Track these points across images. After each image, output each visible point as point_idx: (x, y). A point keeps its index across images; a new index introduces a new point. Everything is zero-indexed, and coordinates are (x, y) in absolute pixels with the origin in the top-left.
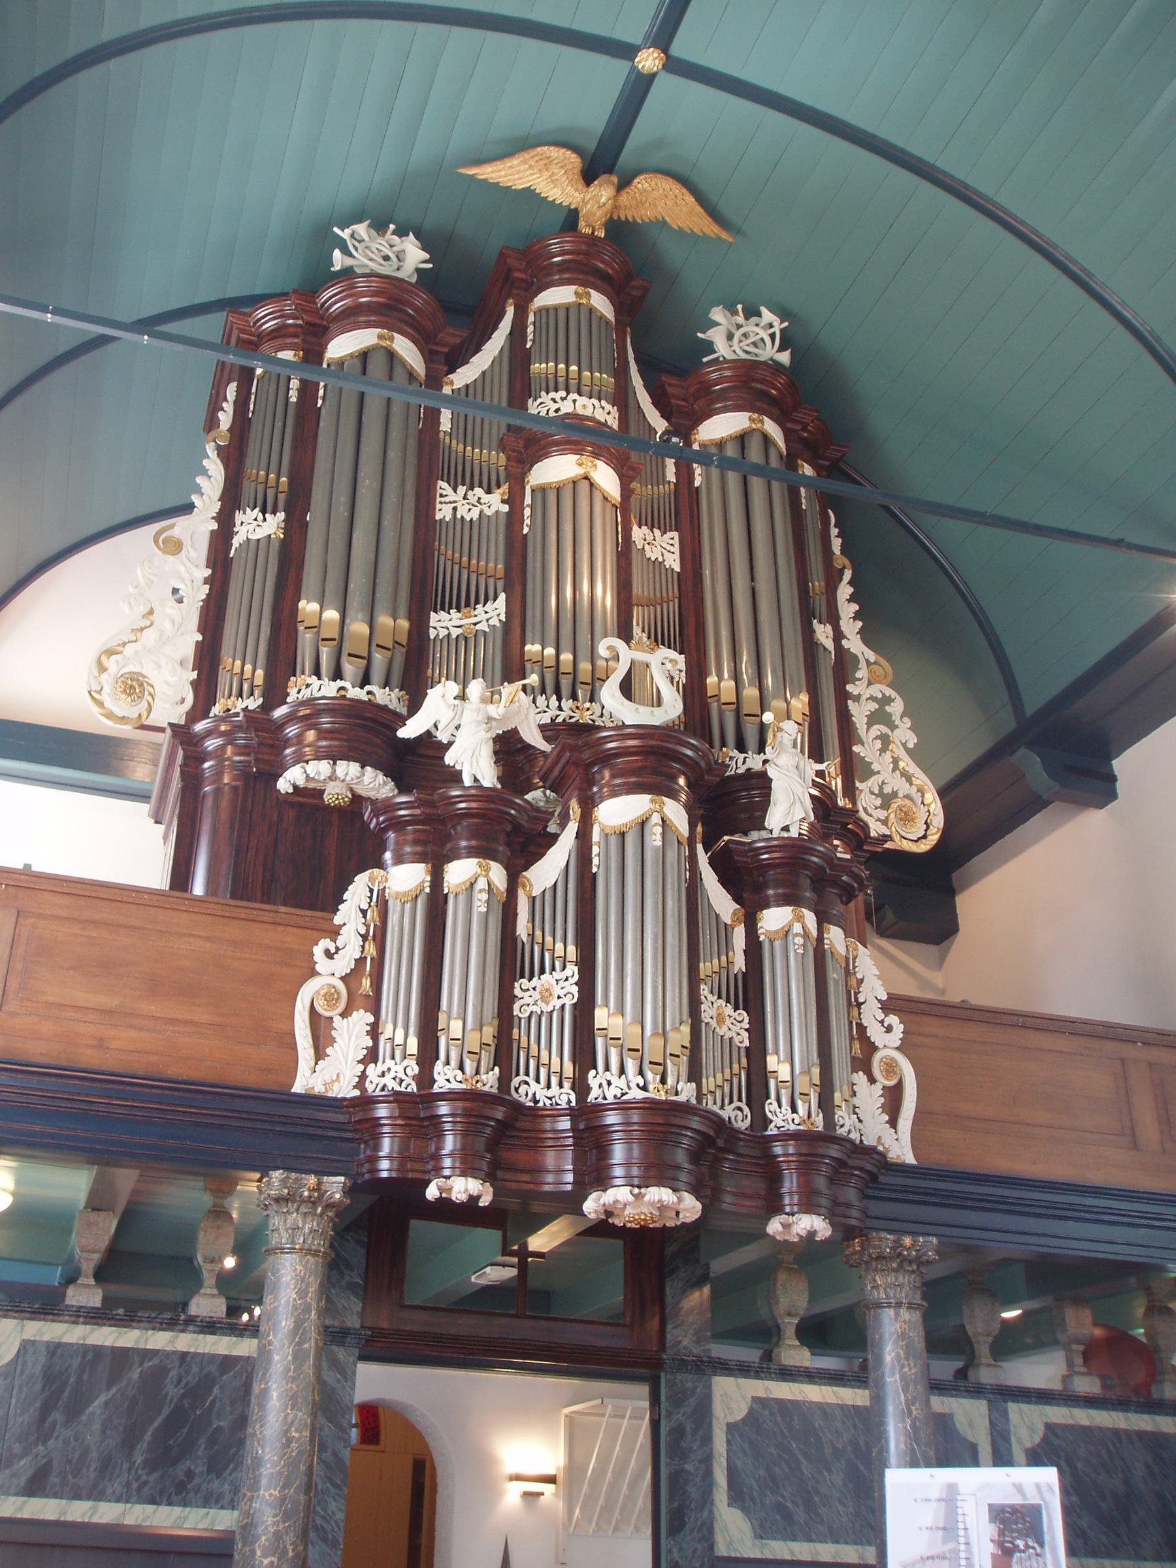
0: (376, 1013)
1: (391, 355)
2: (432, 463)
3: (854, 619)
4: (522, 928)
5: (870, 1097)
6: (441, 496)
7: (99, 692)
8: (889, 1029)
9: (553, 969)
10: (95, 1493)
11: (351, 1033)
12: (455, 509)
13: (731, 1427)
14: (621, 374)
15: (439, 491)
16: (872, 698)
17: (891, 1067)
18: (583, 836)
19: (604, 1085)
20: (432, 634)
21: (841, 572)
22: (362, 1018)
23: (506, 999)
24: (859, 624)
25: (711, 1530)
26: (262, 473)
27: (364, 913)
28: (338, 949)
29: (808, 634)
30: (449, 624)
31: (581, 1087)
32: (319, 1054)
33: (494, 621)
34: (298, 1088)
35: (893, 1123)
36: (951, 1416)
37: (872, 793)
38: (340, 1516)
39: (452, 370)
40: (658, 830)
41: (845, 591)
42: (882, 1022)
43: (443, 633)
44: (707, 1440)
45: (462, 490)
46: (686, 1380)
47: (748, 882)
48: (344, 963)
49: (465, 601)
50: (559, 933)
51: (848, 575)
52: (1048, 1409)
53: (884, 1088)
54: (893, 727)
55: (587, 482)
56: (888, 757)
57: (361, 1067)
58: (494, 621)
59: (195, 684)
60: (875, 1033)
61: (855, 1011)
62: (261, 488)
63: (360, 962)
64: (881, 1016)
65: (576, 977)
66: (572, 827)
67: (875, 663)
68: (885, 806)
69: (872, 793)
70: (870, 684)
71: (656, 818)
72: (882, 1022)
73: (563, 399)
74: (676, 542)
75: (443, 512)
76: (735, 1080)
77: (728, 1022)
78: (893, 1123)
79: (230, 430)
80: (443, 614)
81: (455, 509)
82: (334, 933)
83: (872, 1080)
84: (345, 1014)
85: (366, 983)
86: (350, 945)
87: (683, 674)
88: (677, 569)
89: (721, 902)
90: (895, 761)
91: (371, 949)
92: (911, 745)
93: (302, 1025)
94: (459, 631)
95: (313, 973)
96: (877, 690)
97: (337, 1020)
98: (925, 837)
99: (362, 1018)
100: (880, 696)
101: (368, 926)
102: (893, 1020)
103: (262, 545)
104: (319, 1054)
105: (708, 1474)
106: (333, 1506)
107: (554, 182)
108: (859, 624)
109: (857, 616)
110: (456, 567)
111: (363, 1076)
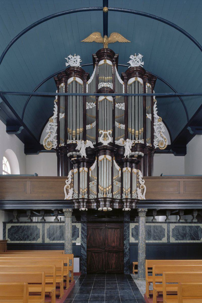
0: (74, 188)
1: (76, 82)
2: (85, 98)
3: (156, 111)
4: (90, 175)
5: (139, 191)
6: (87, 105)
8: (143, 181)
9: (93, 181)
10: (60, 240)
11: (71, 191)
12: (89, 107)
13: (132, 229)
14: (114, 75)
15: (87, 104)
16: (158, 125)
17: (142, 187)
18: (97, 161)
19: (100, 195)
20: (87, 129)
21: (155, 102)
22: (72, 189)
23: (88, 185)
24: (157, 112)
25: (129, 240)
27: (71, 176)
28: (68, 181)
29: (145, 116)
30: (89, 127)
31: (97, 196)
32: (67, 194)
33: (95, 126)
34: (65, 199)
35: (143, 194)
36: (162, 226)
37: (156, 141)
38: (86, 241)
39: (88, 81)
40: (106, 160)
41: (155, 106)
42: (142, 181)
43: (88, 128)
44: (129, 230)
45: (90, 103)
46: (126, 224)
47: (121, 164)
48: (69, 182)
49: (91, 123)
50: (95, 176)
51: (156, 103)
52: (176, 224)
53: (142, 190)
54: (161, 129)
55: (106, 99)
57: (72, 195)
58: (95, 126)
59: (57, 142)
60: (141, 182)
61: (138, 180)
63: (72, 182)
64: (142, 180)
65: (96, 181)
66: (96, 160)
69: (156, 141)
70: (158, 122)
71: (105, 158)
72: (142, 181)
74: (124, 105)
75: (87, 108)
76: (119, 192)
77: (118, 184)
78: (143, 194)
79: (57, 99)
80: (88, 125)
81: (89, 107)
82: (68, 179)
83: (140, 189)
84: (70, 189)
85: (72, 185)
86: (70, 180)
87: (124, 128)
88: (124, 110)
89: (117, 167)
90: (161, 135)
91: (73, 180)
94: (90, 128)
95: (66, 184)
96: (159, 123)
97: (69, 190)
98: (164, 147)
99: (72, 189)
100: (159, 124)
101: (72, 177)
102: (143, 180)
103: (63, 119)
104: (67, 194)
105: (129, 234)
106: (85, 240)
108: (157, 112)
109: (157, 110)
110: (90, 117)
111: (73, 196)
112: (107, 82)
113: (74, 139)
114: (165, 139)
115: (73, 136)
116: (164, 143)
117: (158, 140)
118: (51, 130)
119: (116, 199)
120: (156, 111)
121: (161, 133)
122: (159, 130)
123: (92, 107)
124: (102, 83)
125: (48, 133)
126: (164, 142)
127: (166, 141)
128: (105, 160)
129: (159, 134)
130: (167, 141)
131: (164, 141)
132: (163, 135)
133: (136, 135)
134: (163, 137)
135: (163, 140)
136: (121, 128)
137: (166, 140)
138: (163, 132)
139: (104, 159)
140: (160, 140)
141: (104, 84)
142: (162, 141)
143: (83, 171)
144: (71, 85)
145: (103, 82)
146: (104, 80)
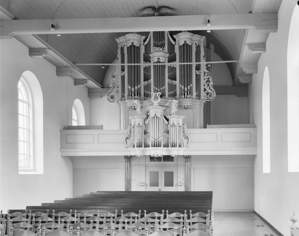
3: (205, 66)
7: (109, 99)
16: (207, 78)
26: (157, 42)
37: (205, 93)
45: (146, 62)
56: (208, 87)
62: (156, 45)
67: (208, 72)
68: (207, 95)
69: (205, 93)
70: (207, 76)
73: (156, 48)
90: (210, 88)
92: (212, 85)
93: (158, 29)
100: (208, 78)
107: (150, 12)
112: (160, 47)
113: (133, 95)
114: (213, 91)
115: (132, 93)
116: (213, 94)
117: (207, 92)
118: (114, 85)
119: (34, 216)
120: (205, 66)
121: (210, 86)
122: (208, 83)
123: (148, 66)
124: (156, 47)
125: (111, 88)
126: (212, 94)
127: (214, 93)
128: (155, 118)
129: (208, 86)
130: (215, 93)
131: (212, 93)
132: (212, 88)
133: (185, 91)
134: (211, 90)
135: (212, 92)
136: (173, 83)
137: (214, 93)
138: (211, 85)
139: (154, 117)
140: (209, 93)
141: (157, 48)
142: (211, 93)
143: (139, 126)
144: (130, 48)
145: (156, 47)
146: (157, 45)
